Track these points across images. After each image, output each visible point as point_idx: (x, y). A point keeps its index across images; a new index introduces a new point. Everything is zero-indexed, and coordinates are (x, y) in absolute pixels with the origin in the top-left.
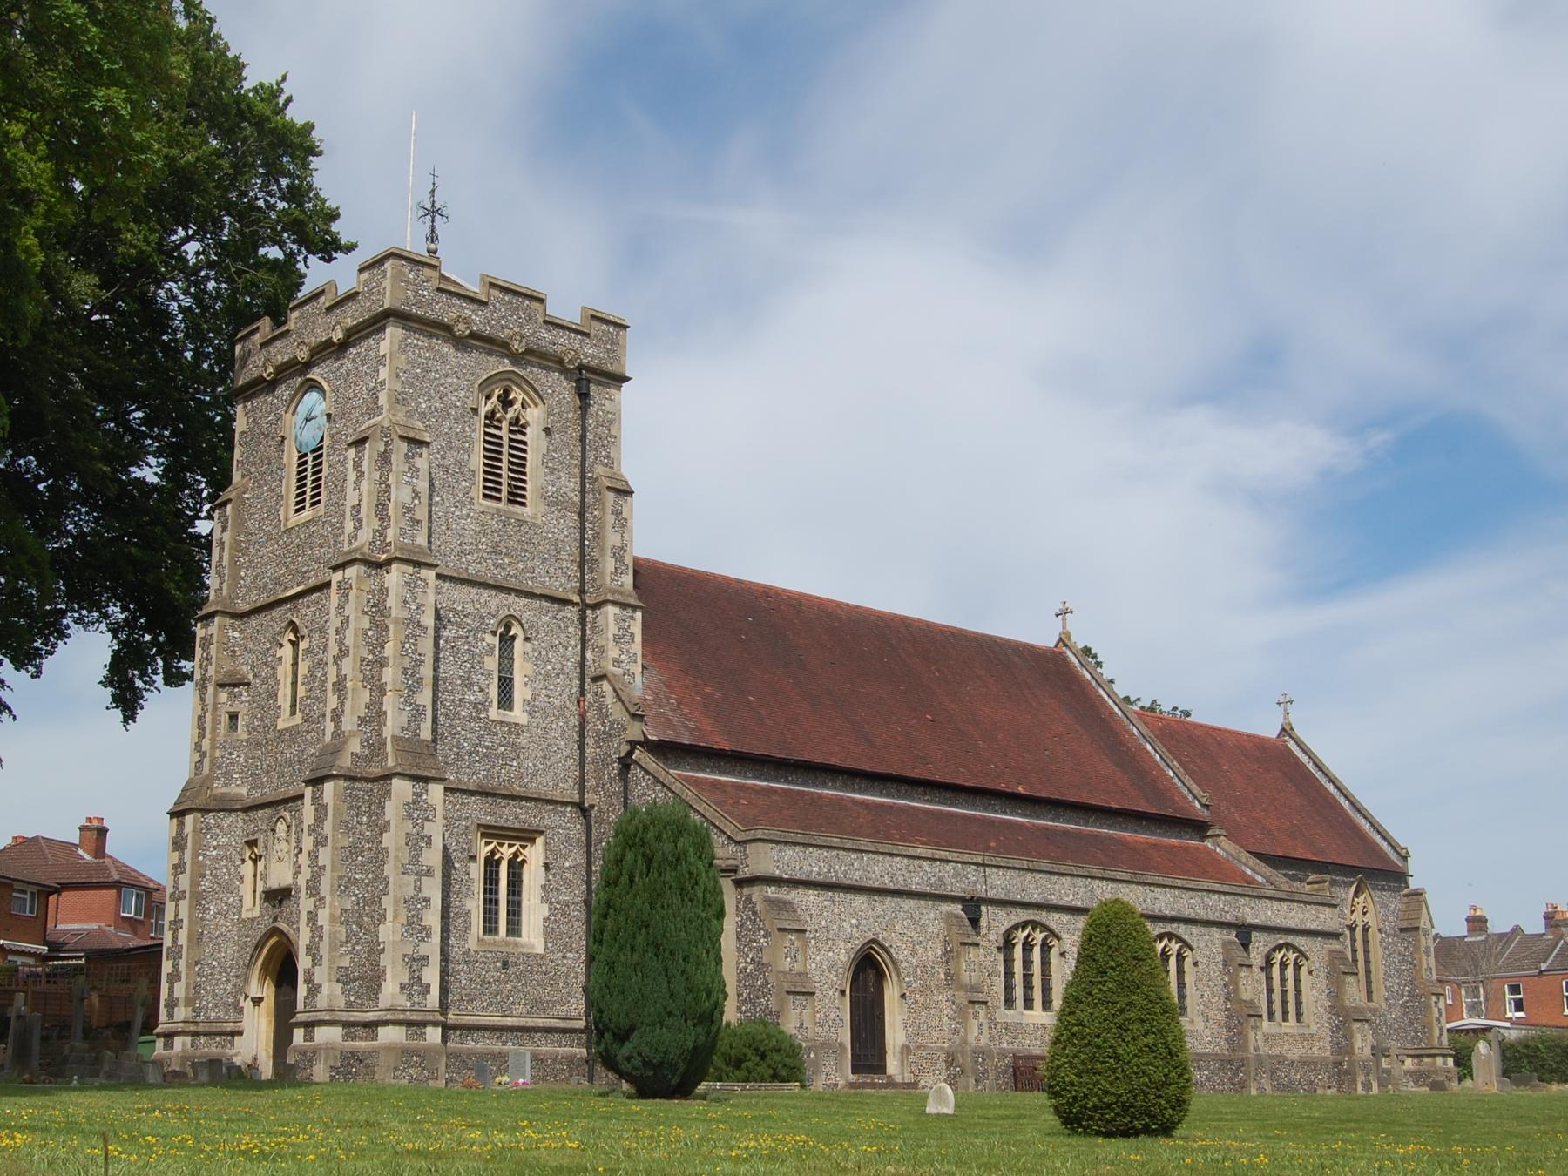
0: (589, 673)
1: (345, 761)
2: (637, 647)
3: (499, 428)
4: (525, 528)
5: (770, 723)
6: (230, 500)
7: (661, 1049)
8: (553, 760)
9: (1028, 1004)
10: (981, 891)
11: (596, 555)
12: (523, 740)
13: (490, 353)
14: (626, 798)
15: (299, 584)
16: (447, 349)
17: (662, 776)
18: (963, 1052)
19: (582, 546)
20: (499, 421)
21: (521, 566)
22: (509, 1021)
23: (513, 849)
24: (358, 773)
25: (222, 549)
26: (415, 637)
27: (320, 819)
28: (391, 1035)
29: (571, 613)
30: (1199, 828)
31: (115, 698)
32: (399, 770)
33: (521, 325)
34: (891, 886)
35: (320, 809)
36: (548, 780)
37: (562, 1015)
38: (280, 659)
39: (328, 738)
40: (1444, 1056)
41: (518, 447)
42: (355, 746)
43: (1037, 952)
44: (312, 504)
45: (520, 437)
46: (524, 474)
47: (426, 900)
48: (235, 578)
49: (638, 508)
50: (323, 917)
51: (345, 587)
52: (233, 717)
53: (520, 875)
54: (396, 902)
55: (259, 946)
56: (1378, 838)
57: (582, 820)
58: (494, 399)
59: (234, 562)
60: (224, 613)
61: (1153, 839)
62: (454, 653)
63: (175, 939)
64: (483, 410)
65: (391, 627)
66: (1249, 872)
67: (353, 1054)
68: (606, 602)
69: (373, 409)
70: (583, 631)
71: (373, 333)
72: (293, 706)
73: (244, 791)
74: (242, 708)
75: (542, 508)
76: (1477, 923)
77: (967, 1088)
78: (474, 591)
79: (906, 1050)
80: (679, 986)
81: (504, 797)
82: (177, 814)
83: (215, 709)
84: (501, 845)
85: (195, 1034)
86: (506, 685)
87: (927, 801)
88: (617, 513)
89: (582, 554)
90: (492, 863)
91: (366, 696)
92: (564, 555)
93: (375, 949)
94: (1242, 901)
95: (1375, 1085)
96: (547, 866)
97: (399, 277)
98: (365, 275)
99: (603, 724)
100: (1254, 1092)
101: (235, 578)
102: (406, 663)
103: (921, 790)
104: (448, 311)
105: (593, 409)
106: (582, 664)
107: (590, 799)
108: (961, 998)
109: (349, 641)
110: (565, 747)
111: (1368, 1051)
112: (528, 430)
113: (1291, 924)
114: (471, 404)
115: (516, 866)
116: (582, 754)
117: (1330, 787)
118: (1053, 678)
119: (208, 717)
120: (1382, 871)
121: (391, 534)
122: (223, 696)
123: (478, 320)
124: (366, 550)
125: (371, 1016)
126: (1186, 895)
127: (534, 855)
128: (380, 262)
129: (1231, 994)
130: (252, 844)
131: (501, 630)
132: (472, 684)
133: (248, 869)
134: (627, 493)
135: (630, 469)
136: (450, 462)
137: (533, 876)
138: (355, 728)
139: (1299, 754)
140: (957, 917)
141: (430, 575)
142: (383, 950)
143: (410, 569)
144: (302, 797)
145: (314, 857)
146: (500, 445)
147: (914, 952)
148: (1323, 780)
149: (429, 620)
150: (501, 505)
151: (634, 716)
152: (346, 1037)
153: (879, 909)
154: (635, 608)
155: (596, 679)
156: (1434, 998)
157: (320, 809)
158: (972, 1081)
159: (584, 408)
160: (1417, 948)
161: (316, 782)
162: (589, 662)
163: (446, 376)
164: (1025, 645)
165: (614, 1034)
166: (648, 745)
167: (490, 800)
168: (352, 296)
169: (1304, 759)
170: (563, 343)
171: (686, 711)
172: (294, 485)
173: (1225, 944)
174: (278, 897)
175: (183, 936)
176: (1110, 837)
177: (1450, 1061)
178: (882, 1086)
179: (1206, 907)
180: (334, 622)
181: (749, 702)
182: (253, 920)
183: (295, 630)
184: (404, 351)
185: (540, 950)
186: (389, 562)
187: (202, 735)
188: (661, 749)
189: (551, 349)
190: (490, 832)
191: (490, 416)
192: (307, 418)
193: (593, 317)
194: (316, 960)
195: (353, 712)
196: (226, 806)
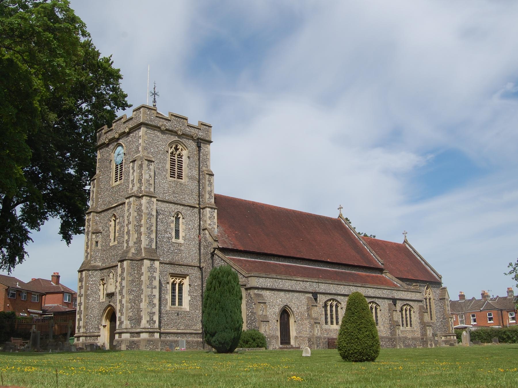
0: (202, 228)
1: (130, 255)
2: (216, 220)
4: (182, 186)
9: (332, 323)
10: (317, 290)
11: (203, 193)
12: (182, 248)
13: (172, 135)
14: (213, 265)
16: (159, 134)
18: (313, 338)
19: (199, 190)
22: (179, 331)
25: (93, 193)
27: (122, 272)
29: (196, 210)
30: (381, 270)
31: (64, 238)
33: (181, 127)
35: (123, 269)
39: (125, 248)
40: (453, 336)
41: (180, 162)
42: (133, 250)
45: (181, 159)
47: (154, 296)
48: (97, 202)
49: (215, 179)
51: (129, 204)
52: (97, 242)
53: (182, 288)
54: (145, 296)
55: (105, 310)
56: (432, 272)
58: (173, 148)
59: (97, 196)
61: (368, 274)
62: (162, 223)
63: (80, 308)
64: (170, 151)
68: (206, 207)
69: (137, 151)
72: (115, 239)
73: (100, 264)
74: (99, 240)
75: (187, 180)
76: (462, 297)
78: (167, 204)
79: (296, 337)
81: (177, 265)
82: (80, 271)
83: (91, 240)
86: (177, 232)
88: (209, 181)
89: (199, 193)
90: (174, 284)
91: (136, 236)
93: (139, 310)
94: (394, 292)
95: (433, 345)
96: (190, 285)
97: (145, 113)
98: (135, 113)
100: (398, 348)
104: (159, 123)
105: (202, 151)
106: (200, 225)
107: (202, 265)
108: (312, 321)
109: (131, 220)
110: (195, 250)
111: (431, 335)
113: (408, 298)
114: (166, 150)
115: (181, 285)
116: (200, 252)
117: (419, 258)
118: (338, 227)
119: (89, 242)
120: (434, 282)
121: (143, 188)
122: (94, 236)
123: (168, 125)
124: (136, 193)
125: (138, 330)
126: (377, 290)
127: (186, 282)
129: (391, 319)
130: (103, 280)
135: (213, 168)
136: (160, 167)
137: (186, 288)
140: (311, 298)
141: (154, 200)
143: (149, 198)
144: (117, 266)
145: (121, 284)
147: (298, 309)
148: (416, 256)
149: (154, 213)
150: (175, 179)
151: (215, 240)
153: (288, 296)
154: (215, 209)
155: (204, 230)
157: (123, 269)
158: (316, 346)
159: (199, 150)
160: (445, 304)
161: (122, 261)
162: (202, 225)
163: (159, 142)
164: (329, 218)
168: (131, 119)
169: (411, 250)
170: (193, 131)
173: (389, 304)
174: (110, 295)
176: (355, 274)
177: (455, 337)
179: (383, 294)
180: (127, 214)
182: (103, 302)
183: (115, 217)
184: (146, 135)
186: (142, 196)
187: (87, 248)
188: (223, 250)
189: (189, 133)
190: (173, 275)
191: (172, 153)
192: (118, 154)
193: (202, 124)
196: (95, 269)
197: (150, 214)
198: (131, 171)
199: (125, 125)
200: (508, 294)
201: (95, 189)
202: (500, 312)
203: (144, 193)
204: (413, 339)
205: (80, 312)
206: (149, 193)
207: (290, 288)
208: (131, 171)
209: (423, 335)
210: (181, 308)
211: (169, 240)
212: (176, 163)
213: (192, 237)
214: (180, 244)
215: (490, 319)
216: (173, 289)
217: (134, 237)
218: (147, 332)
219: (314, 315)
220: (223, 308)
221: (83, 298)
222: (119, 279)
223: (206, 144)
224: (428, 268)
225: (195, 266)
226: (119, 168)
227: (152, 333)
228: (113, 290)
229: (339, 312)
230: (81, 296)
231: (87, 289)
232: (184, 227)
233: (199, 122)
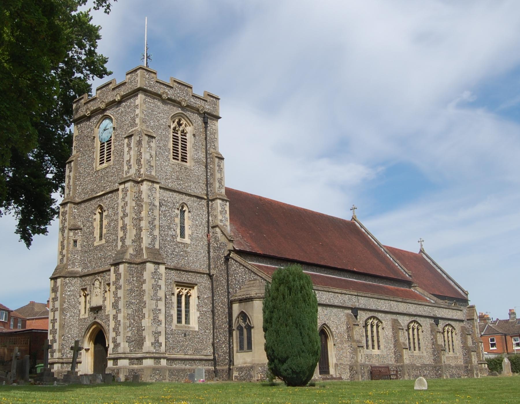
0: (211, 224)
1: (128, 257)
2: (228, 216)
3: (177, 134)
4: (187, 170)
5: (273, 244)
6: (73, 161)
7: (300, 366)
8: (199, 257)
9: (373, 348)
10: (357, 305)
11: (211, 181)
12: (189, 250)
13: (174, 106)
14: (227, 271)
15: (102, 191)
16: (160, 104)
17: (243, 262)
18: (356, 366)
19: (207, 178)
20: (177, 131)
21: (186, 185)
22: (187, 357)
23: (187, 291)
24: (132, 261)
25: (70, 179)
26: (153, 210)
27: (118, 279)
28: (148, 363)
29: (204, 202)
30: (409, 284)
31: (22, 237)
32: (149, 260)
33: (184, 96)
34: (329, 303)
35: (118, 276)
36: (198, 264)
37: (205, 354)
38: (95, 219)
39: (119, 248)
40: (485, 364)
41: (184, 141)
42: (131, 251)
43: (375, 327)
44: (107, 161)
45: (184, 137)
46: (186, 151)
47: (160, 310)
48: (75, 189)
49: (226, 164)
50: (120, 317)
51: (125, 191)
52: (75, 242)
53: (189, 301)
54: (149, 311)
55: (88, 329)
56: (457, 288)
57: (210, 280)
58: (176, 123)
59: (75, 184)
60: (71, 202)
61: (396, 287)
62: (165, 216)
63: (53, 326)
64: (172, 127)
65: (144, 206)
66: (428, 299)
67: (133, 370)
68: (217, 198)
69: (133, 124)
70: (208, 209)
71: (132, 97)
72: (101, 237)
73: (80, 270)
74: (79, 238)
75: (193, 163)
77: (359, 379)
78: (171, 193)
79: (336, 365)
80: (307, 340)
81: (183, 271)
82: (54, 278)
83: (68, 238)
84: (182, 289)
85: (62, 363)
86: (182, 229)
87: (326, 274)
88: (219, 166)
89: (207, 181)
90: (179, 296)
91: (134, 232)
92: (201, 181)
93: (140, 329)
94: (435, 309)
95: (479, 374)
96: (198, 297)
97: (143, 76)
98: (129, 76)
99: (217, 244)
100: (445, 378)
101: (75, 189)
102: (150, 219)
103: (323, 269)
104: (160, 90)
105: (209, 128)
106: (208, 222)
107: (212, 272)
108: (354, 345)
109: (128, 211)
110: (203, 253)
111: (476, 362)
112: (187, 135)
113: (449, 317)
114: (168, 124)
115: (188, 297)
116: (209, 255)
117: (439, 270)
119: (65, 242)
120: (460, 299)
121: (142, 171)
122: (71, 234)
123: (170, 93)
124: (133, 177)
125: (139, 355)
126: (418, 306)
127: (194, 293)
128: (136, 70)
129: (434, 343)
130: (84, 290)
131: (180, 208)
132: (171, 228)
133: (82, 299)
134: (221, 159)
135: (222, 150)
136: (161, 145)
137: (194, 301)
138: (131, 244)
139: (427, 259)
140: (350, 315)
141: (157, 186)
142: (144, 330)
144: (109, 270)
145: (115, 294)
146: (178, 140)
147: (337, 328)
148: (436, 268)
149: (157, 204)
151: (230, 241)
152: (155, 363)
153: (326, 312)
154: (226, 201)
155: (213, 227)
156: (480, 344)
157: (118, 276)
158: (360, 377)
159: (206, 127)
160: (474, 326)
161: (116, 265)
162: (211, 221)
163: (159, 113)
164: (342, 220)
165: (279, 360)
166: (235, 251)
167: (178, 272)
168: (124, 84)
169: (429, 261)
171: (245, 239)
172: (99, 154)
173: (431, 324)
174: (96, 310)
175: (57, 326)
176: (383, 287)
177: (486, 365)
178: (328, 379)
179: (425, 311)
181: (264, 237)
182: (85, 319)
183: (101, 208)
184: (145, 103)
185: (197, 329)
186: (142, 181)
187: (63, 247)
188: (240, 253)
189: (195, 105)
190: (179, 284)
191: (174, 129)
192: (104, 129)
193: (208, 95)
194: (118, 334)
195: (130, 238)
196: (73, 275)
197: (152, 204)
198: (126, 149)
199: (115, 92)
200: (510, 317)
201: (72, 174)
202: (504, 337)
203: (144, 177)
204: (457, 367)
205: (54, 332)
206: (150, 177)
207: (327, 302)
208: (126, 149)
209: (466, 363)
210: (189, 327)
211: (174, 239)
212: (180, 142)
213: (200, 236)
214: (185, 245)
215: (493, 345)
216: (179, 302)
217: (132, 233)
218: (151, 358)
219: (356, 337)
220: (297, 324)
221: (57, 314)
222: (113, 288)
223: (213, 120)
224: (451, 282)
225: (204, 274)
226: (106, 146)
227: (157, 359)
228: (100, 303)
229: (380, 333)
230: (54, 310)
231: (63, 302)
232: (190, 223)
233: (205, 92)
